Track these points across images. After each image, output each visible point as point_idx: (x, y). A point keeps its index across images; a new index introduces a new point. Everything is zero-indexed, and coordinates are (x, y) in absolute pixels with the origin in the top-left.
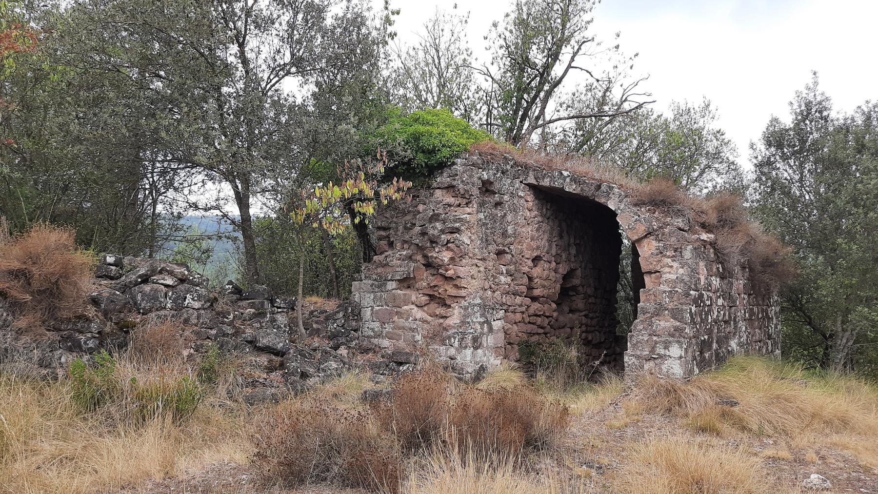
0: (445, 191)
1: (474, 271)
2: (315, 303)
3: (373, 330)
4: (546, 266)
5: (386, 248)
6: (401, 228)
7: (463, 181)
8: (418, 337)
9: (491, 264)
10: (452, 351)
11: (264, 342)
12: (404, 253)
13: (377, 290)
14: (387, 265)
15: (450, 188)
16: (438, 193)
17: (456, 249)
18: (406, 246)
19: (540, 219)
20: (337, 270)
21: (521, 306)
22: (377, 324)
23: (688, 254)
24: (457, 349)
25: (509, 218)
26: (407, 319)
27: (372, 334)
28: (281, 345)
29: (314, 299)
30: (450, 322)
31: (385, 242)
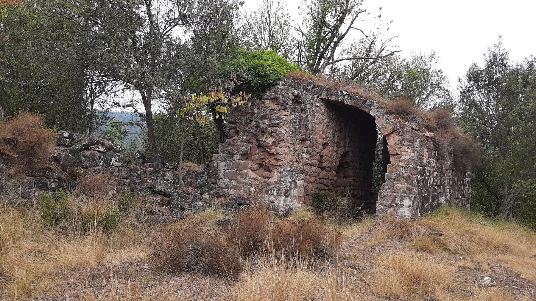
0: (271, 101)
1: (287, 150)
2: (190, 166)
3: (224, 184)
4: (331, 149)
5: (234, 134)
6: (243, 123)
7: (282, 95)
8: (252, 189)
9: (298, 146)
10: (272, 198)
11: (158, 188)
12: (245, 138)
13: (227, 160)
14: (234, 145)
15: (274, 99)
16: (267, 102)
17: (276, 136)
18: (246, 134)
20: (203, 147)
21: (314, 172)
22: (228, 180)
23: (417, 144)
24: (275, 197)
25: (310, 119)
26: (246, 178)
27: (224, 186)
28: (169, 190)
29: (189, 164)
30: (272, 180)
31: (234, 131)
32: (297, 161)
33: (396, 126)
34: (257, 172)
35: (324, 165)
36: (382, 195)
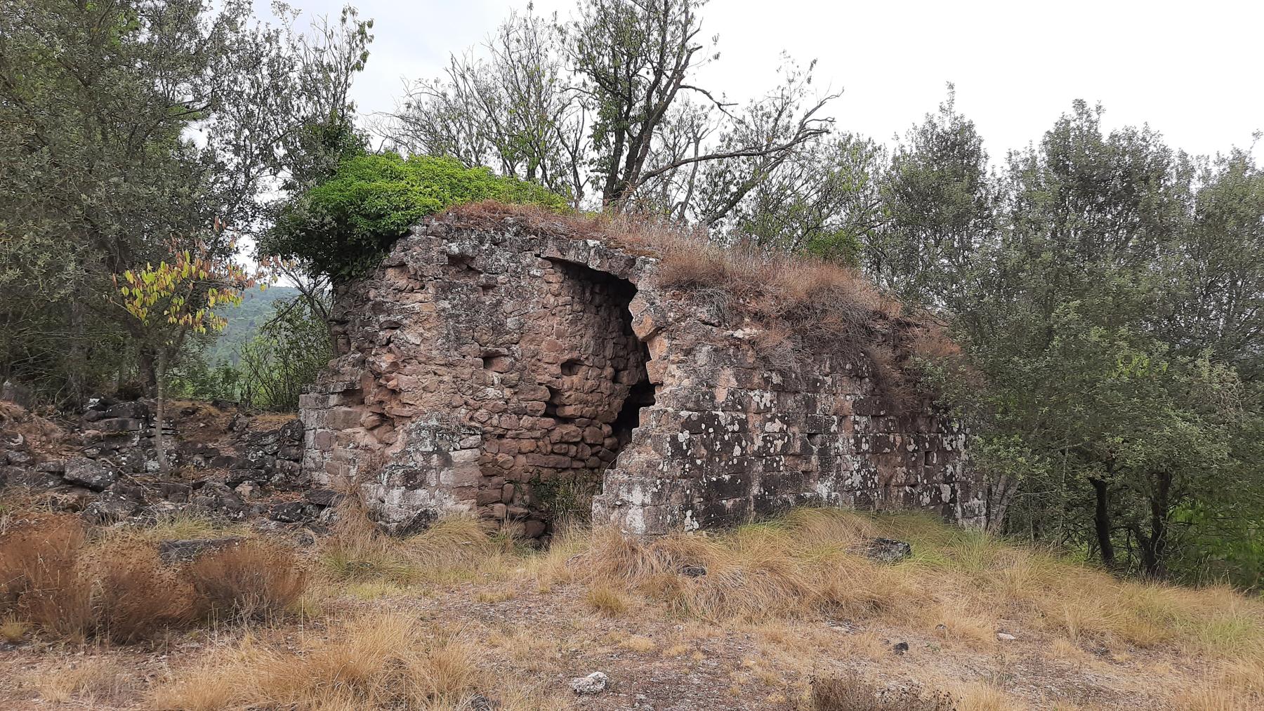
1: (429, 380)
4: (593, 373)
9: (468, 370)
11: (71, 473)
15: (402, 266)
16: (391, 273)
19: (577, 307)
21: (531, 429)
23: (702, 357)
25: (508, 306)
28: (99, 477)
30: (390, 452)
32: (466, 403)
33: (664, 317)
34: (376, 432)
35: (569, 411)
36: (610, 479)
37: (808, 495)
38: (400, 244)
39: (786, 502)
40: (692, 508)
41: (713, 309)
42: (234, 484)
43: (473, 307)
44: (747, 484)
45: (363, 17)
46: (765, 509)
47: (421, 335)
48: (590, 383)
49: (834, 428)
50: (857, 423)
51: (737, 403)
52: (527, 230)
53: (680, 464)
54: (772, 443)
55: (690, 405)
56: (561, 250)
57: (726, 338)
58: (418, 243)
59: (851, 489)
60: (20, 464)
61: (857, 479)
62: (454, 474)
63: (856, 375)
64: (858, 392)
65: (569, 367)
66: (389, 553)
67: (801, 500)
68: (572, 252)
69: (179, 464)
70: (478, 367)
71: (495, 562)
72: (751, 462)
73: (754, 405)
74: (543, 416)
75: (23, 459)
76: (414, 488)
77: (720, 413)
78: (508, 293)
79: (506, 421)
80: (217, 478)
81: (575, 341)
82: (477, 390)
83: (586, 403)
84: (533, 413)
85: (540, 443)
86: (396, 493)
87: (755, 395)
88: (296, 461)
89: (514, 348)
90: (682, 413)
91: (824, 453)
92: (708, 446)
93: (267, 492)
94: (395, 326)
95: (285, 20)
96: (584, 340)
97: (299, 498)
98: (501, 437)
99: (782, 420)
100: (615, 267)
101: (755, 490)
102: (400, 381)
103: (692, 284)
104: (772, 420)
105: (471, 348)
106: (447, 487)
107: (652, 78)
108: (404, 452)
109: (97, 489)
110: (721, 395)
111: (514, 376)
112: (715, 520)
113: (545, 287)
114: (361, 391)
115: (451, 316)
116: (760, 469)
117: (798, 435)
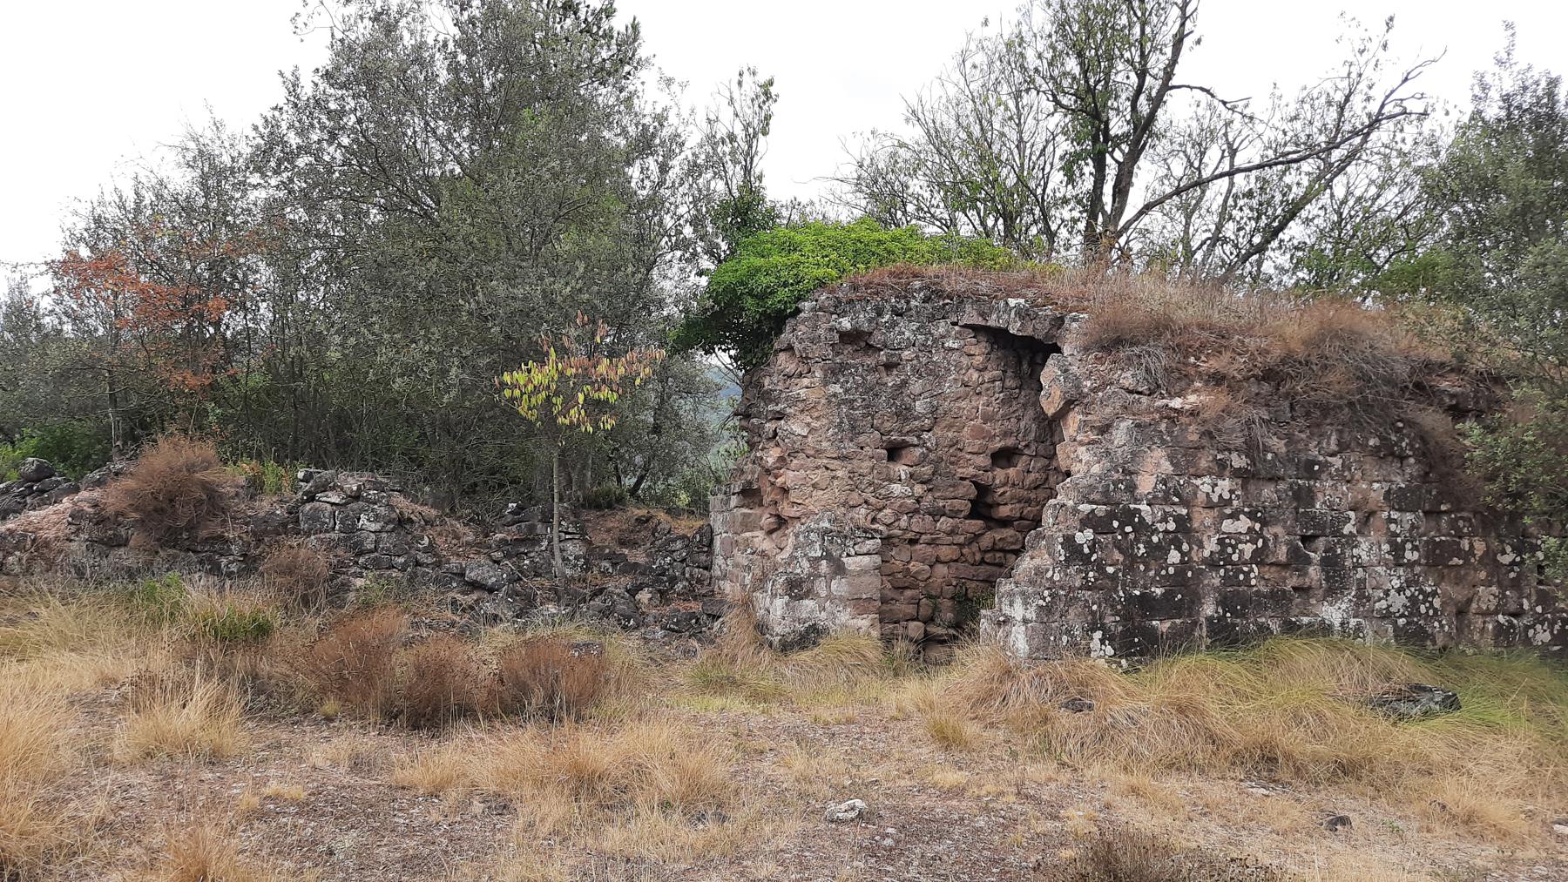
11: (471, 575)
21: (951, 533)
25: (916, 386)
33: (1078, 387)
35: (1004, 511)
37: (1305, 620)
38: (790, 323)
39: (1264, 630)
40: (1103, 628)
41: (1141, 373)
42: (633, 591)
43: (871, 391)
44: (1195, 600)
45: (762, 78)
46: (1225, 637)
47: (808, 424)
48: (1032, 476)
49: (1348, 528)
50: (1395, 521)
51: (1167, 494)
52: (940, 294)
53: (1079, 571)
54: (1234, 547)
55: (1095, 496)
56: (983, 315)
57: (1158, 410)
58: (806, 319)
59: (1387, 615)
60: (428, 565)
61: (1398, 602)
62: (850, 584)
63: (1388, 453)
64: (1398, 479)
65: (1004, 457)
66: (764, 669)
67: (1290, 628)
68: (994, 316)
69: (587, 570)
70: (879, 459)
71: (872, 686)
72: (1199, 574)
73: (1201, 497)
74: (966, 518)
75: (430, 561)
76: (800, 598)
77: (1144, 507)
78: (916, 371)
79: (918, 523)
80: (618, 585)
81: (1010, 425)
82: (880, 486)
83: (1028, 501)
84: (954, 514)
85: (965, 551)
86: (779, 603)
87: (1204, 484)
88: (706, 568)
89: (925, 436)
90: (1081, 507)
91: (1331, 563)
92: (1126, 549)
93: (668, 602)
94: (780, 416)
95: (673, 96)
96: (1022, 424)
97: (696, 607)
98: (913, 542)
99: (1252, 516)
100: (1037, 329)
101: (1209, 609)
102: (788, 477)
103: (1118, 342)
104: (1234, 516)
105: (870, 438)
106: (841, 599)
107: (1134, 79)
108: (792, 557)
109: (491, 590)
110: (1146, 484)
111: (927, 470)
112: (1137, 644)
113: (965, 361)
114: (759, 490)
115: (845, 402)
116: (1216, 582)
117: (1283, 537)
